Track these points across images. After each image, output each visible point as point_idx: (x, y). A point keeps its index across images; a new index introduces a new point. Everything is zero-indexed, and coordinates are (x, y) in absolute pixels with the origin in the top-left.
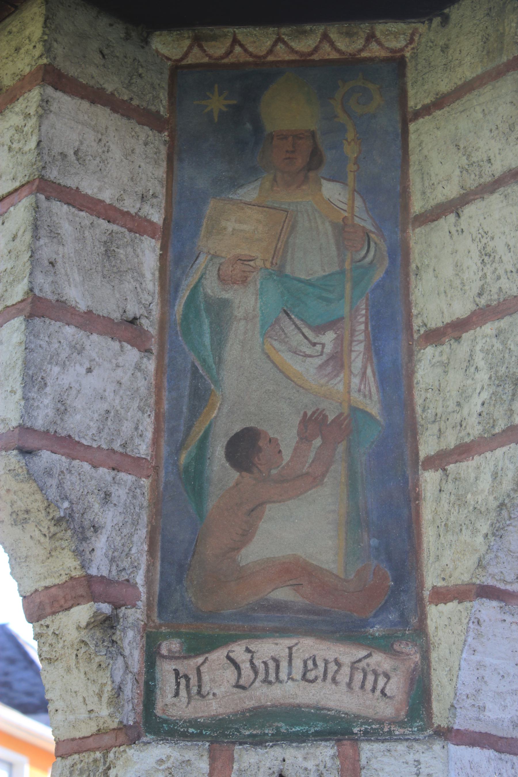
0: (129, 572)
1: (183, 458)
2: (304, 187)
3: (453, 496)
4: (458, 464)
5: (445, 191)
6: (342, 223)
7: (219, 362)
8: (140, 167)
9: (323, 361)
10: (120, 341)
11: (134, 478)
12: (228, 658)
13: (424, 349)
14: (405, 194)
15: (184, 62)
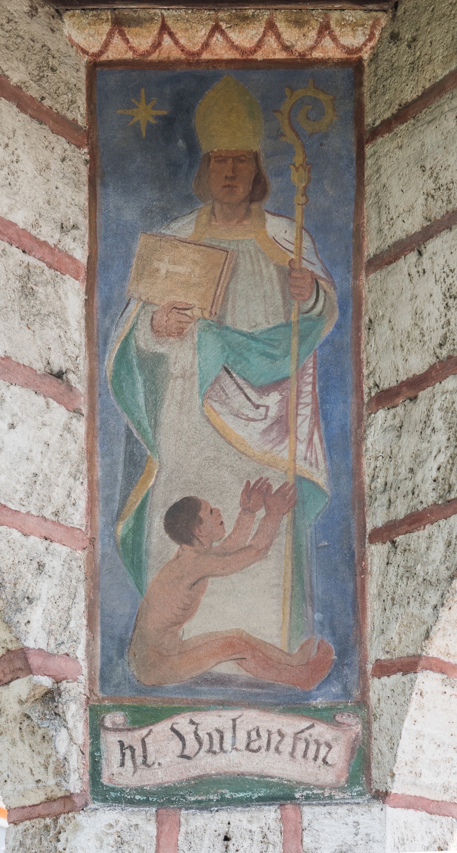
0: (68, 646)
1: (121, 529)
2: (245, 223)
3: (401, 568)
4: (408, 535)
5: (406, 226)
6: (288, 267)
7: (155, 425)
8: (57, 188)
9: (267, 425)
10: (45, 396)
11: (69, 550)
12: (173, 729)
13: (375, 414)
14: (358, 235)
15: (104, 58)
